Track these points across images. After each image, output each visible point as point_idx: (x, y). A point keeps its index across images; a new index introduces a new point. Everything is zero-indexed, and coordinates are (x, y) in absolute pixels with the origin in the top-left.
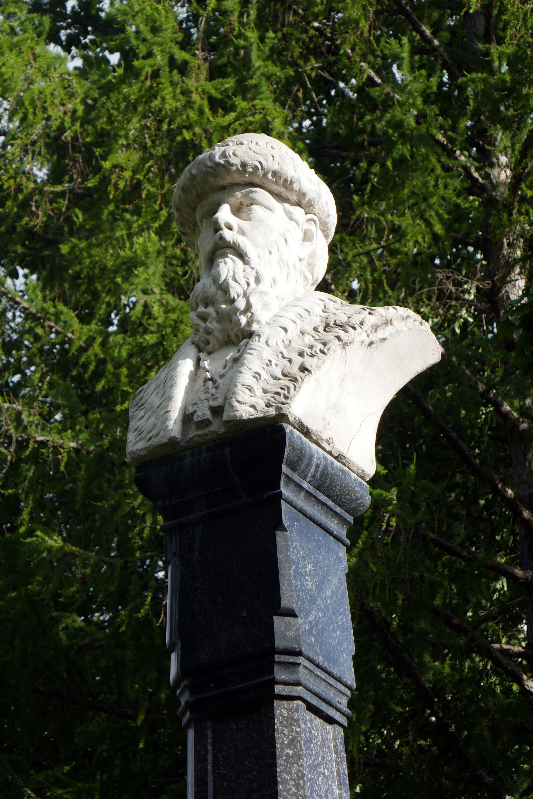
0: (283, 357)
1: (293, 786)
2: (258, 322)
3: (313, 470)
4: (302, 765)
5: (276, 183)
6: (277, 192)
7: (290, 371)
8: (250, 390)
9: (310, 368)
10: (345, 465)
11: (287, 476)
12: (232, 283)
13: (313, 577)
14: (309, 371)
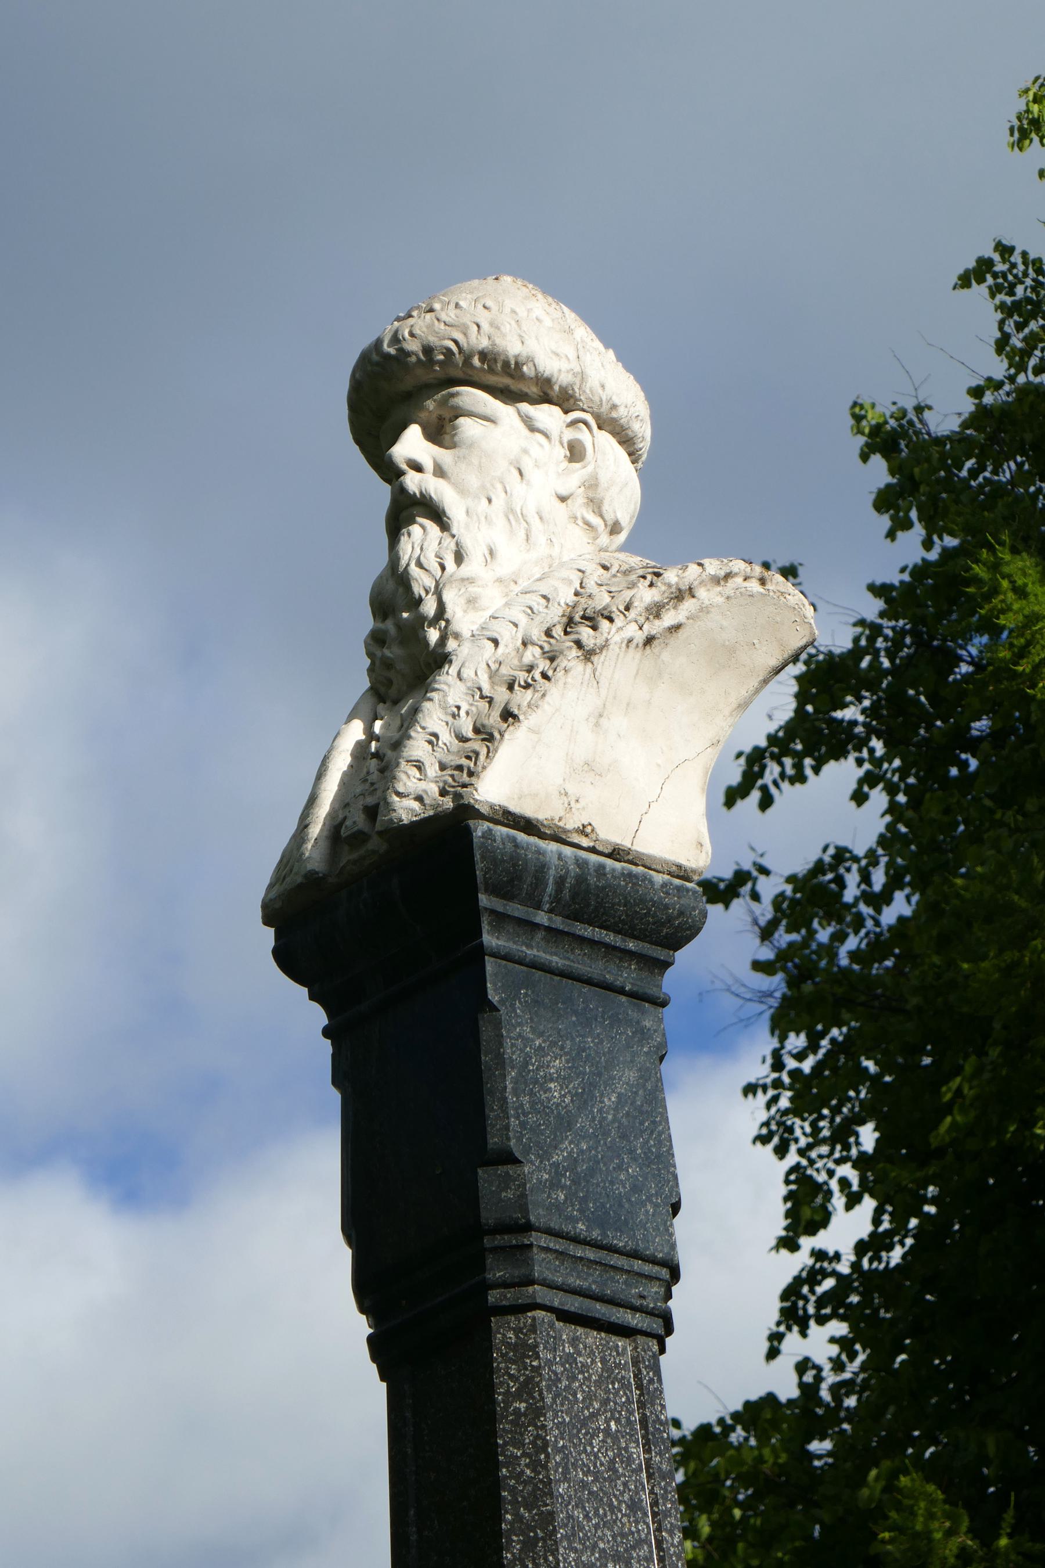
0: (482, 697)
1: (527, 1466)
2: (457, 636)
3: (550, 888)
4: (544, 1427)
5: (491, 370)
6: (500, 386)
7: (486, 722)
8: (419, 768)
9: (516, 712)
10: (636, 865)
11: (492, 912)
12: (414, 570)
13: (564, 1081)
14: (515, 717)
